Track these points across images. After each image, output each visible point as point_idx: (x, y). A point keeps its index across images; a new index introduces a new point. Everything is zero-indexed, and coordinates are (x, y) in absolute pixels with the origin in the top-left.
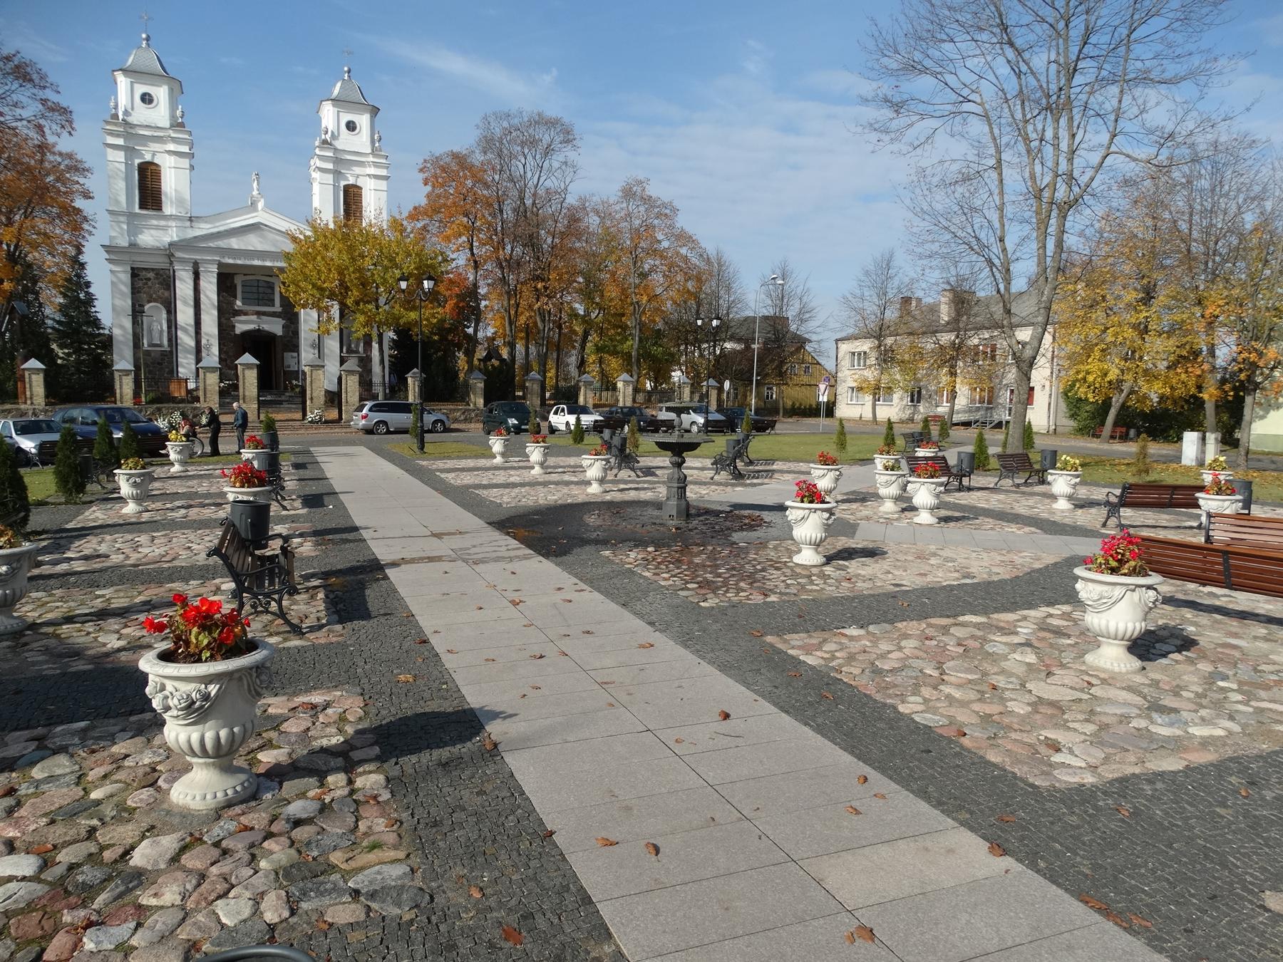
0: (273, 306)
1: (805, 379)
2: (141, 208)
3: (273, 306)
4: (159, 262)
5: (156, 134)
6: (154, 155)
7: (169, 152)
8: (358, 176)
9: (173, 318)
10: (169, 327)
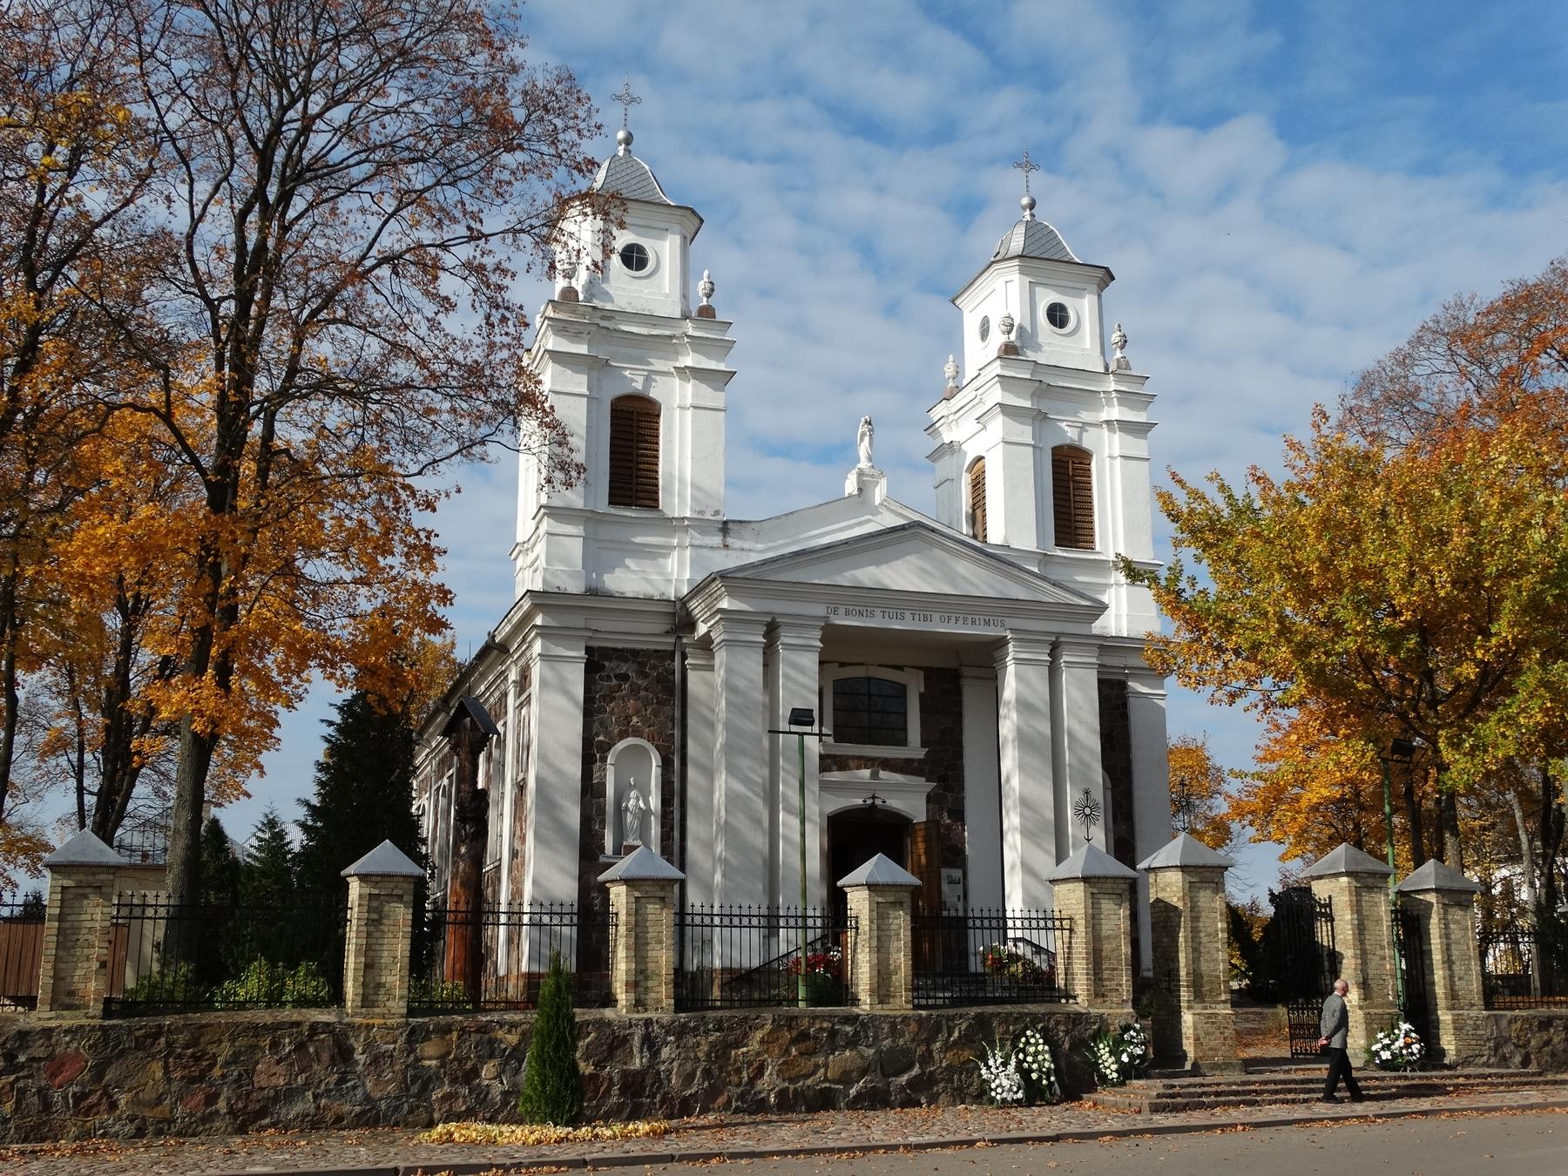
0: (903, 742)
1: (510, 442)
2: (612, 502)
3: (903, 742)
4: (649, 634)
5: (655, 332)
6: (648, 380)
7: (682, 372)
8: (1084, 426)
9: (676, 780)
10: (666, 801)
